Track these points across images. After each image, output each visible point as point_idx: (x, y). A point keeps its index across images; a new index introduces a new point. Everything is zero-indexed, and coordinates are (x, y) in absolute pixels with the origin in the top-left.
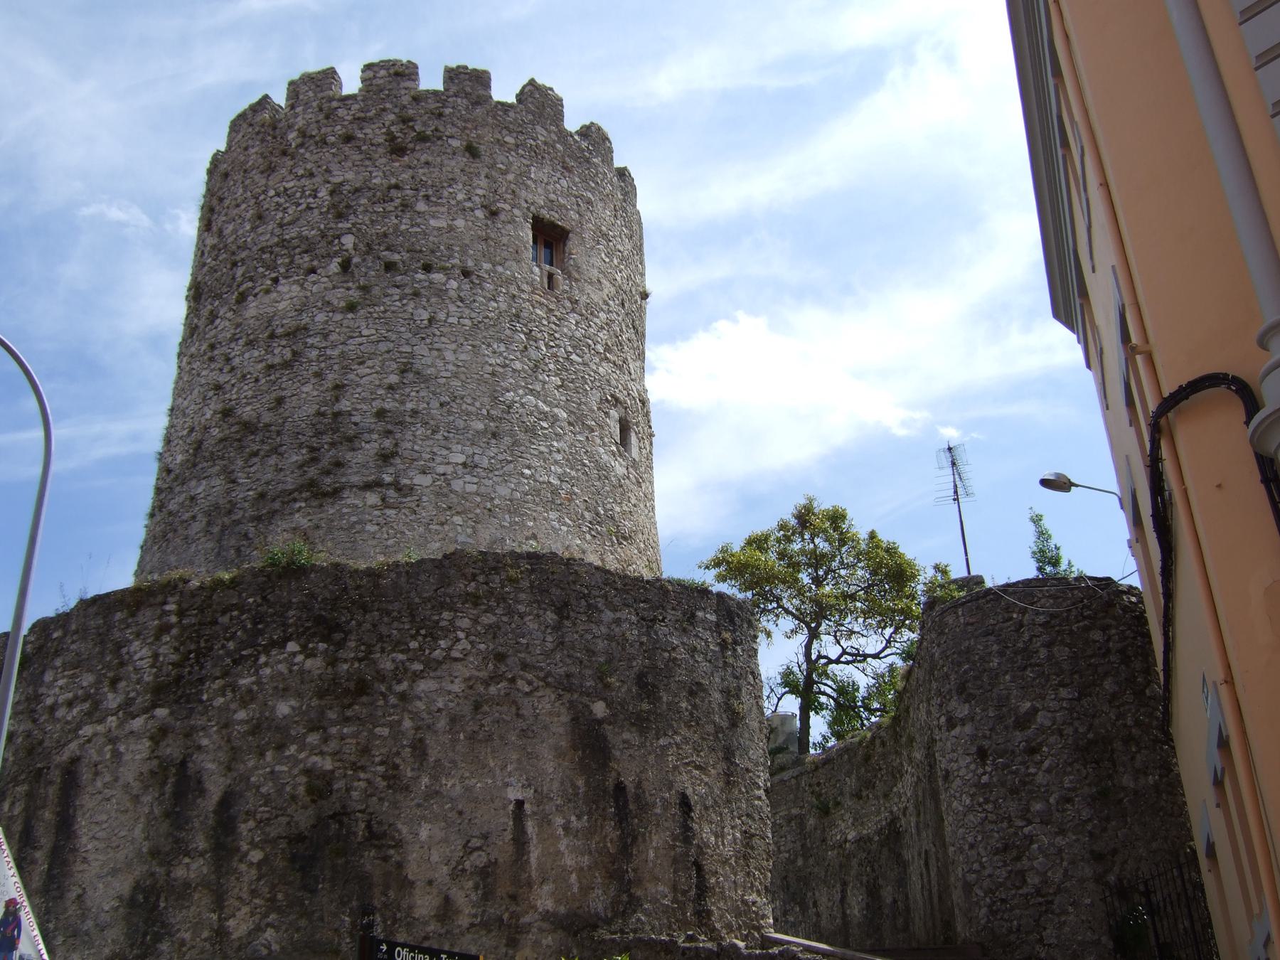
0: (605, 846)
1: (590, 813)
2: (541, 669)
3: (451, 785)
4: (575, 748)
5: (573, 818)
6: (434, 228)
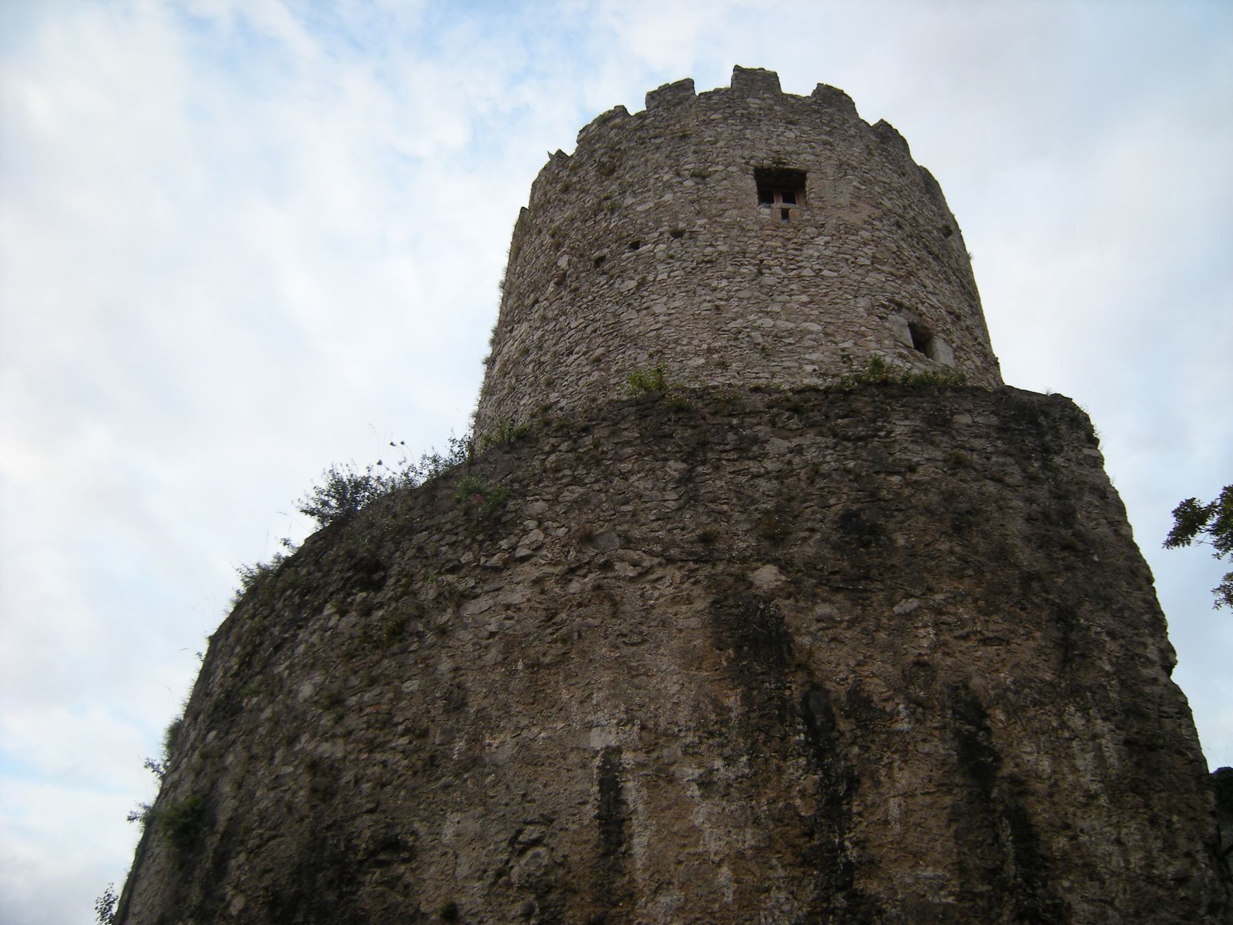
0: (789, 806)
1: (753, 752)
2: (658, 540)
3: (500, 746)
4: (720, 646)
5: (718, 763)
6: (641, 212)
